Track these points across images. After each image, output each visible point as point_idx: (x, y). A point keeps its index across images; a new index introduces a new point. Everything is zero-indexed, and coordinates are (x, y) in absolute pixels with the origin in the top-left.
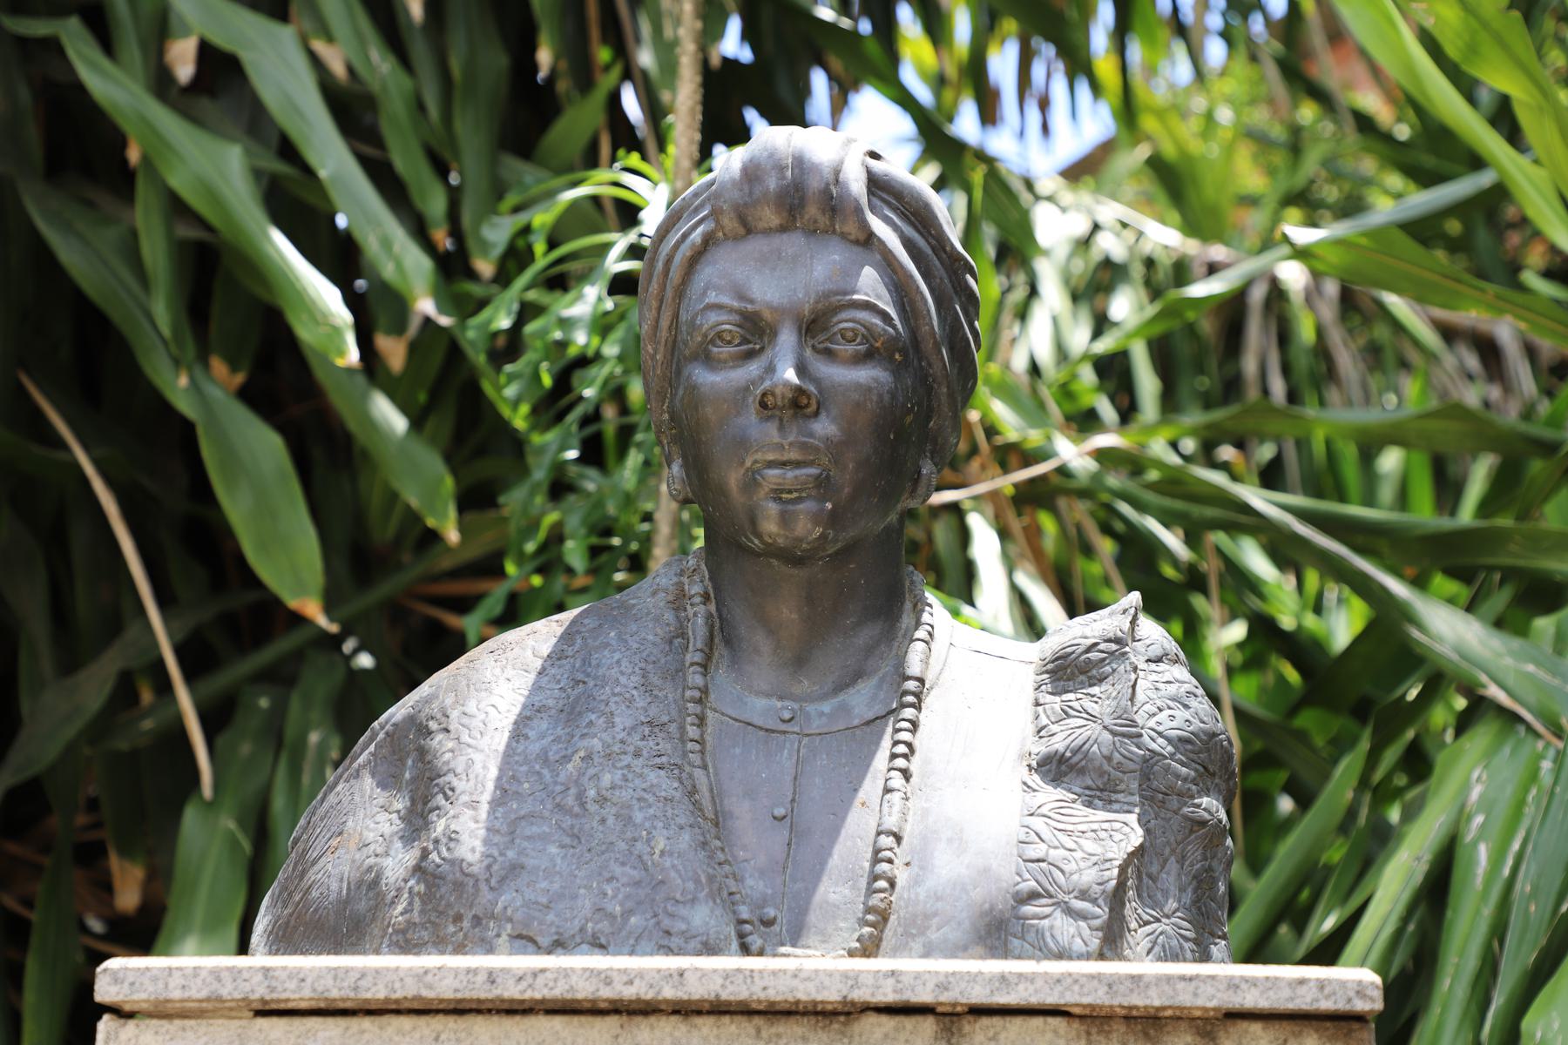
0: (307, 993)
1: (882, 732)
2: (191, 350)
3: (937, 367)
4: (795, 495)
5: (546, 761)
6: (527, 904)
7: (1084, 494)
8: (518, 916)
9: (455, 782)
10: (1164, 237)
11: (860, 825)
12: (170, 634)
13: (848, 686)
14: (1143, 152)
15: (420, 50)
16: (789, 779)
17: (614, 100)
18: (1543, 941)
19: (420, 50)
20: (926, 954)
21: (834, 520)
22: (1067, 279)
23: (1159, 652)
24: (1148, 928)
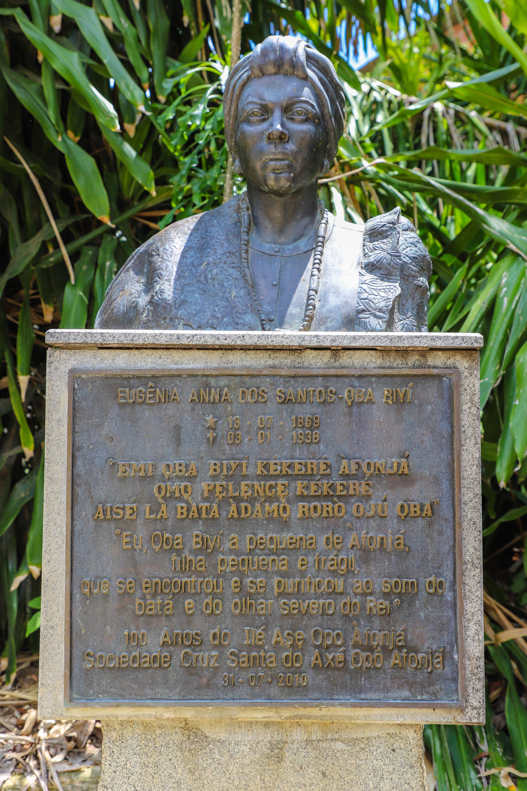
0: (116, 342)
1: (310, 256)
2: (62, 128)
3: (330, 125)
4: (280, 171)
5: (193, 265)
6: (188, 314)
7: (372, 180)
8: (185, 318)
9: (162, 272)
10: (394, 93)
11: (303, 287)
12: (58, 229)
13: (298, 240)
14: (388, 62)
15: (138, 20)
16: (278, 271)
17: (206, 41)
18: (524, 329)
19: (138, 20)
20: (326, 331)
21: (294, 180)
22: (361, 107)
23: (407, 227)
24: (401, 322)
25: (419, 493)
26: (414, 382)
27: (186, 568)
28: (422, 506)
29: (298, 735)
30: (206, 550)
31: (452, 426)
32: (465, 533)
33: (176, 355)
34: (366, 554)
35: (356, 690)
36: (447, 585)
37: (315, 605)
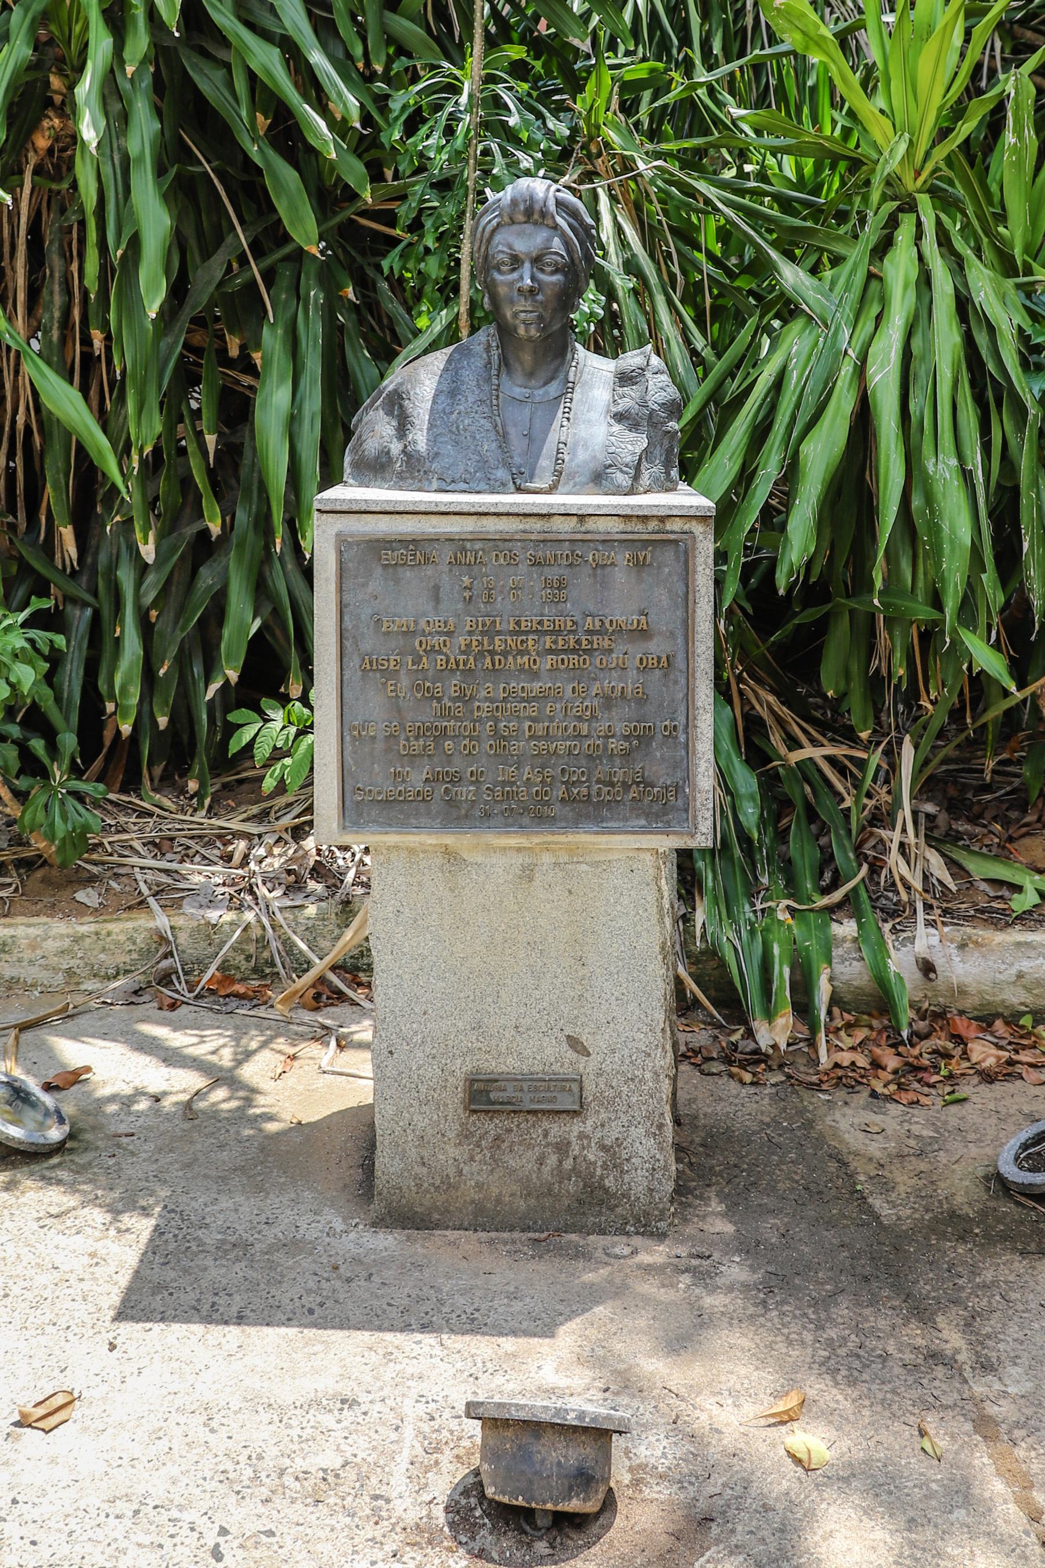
11: (553, 438)
25: (656, 647)
26: (652, 543)
27: (446, 714)
28: (659, 659)
29: (547, 859)
30: (463, 698)
31: (687, 587)
32: (698, 682)
33: (434, 519)
34: (608, 701)
35: (599, 819)
36: (681, 728)
37: (562, 746)
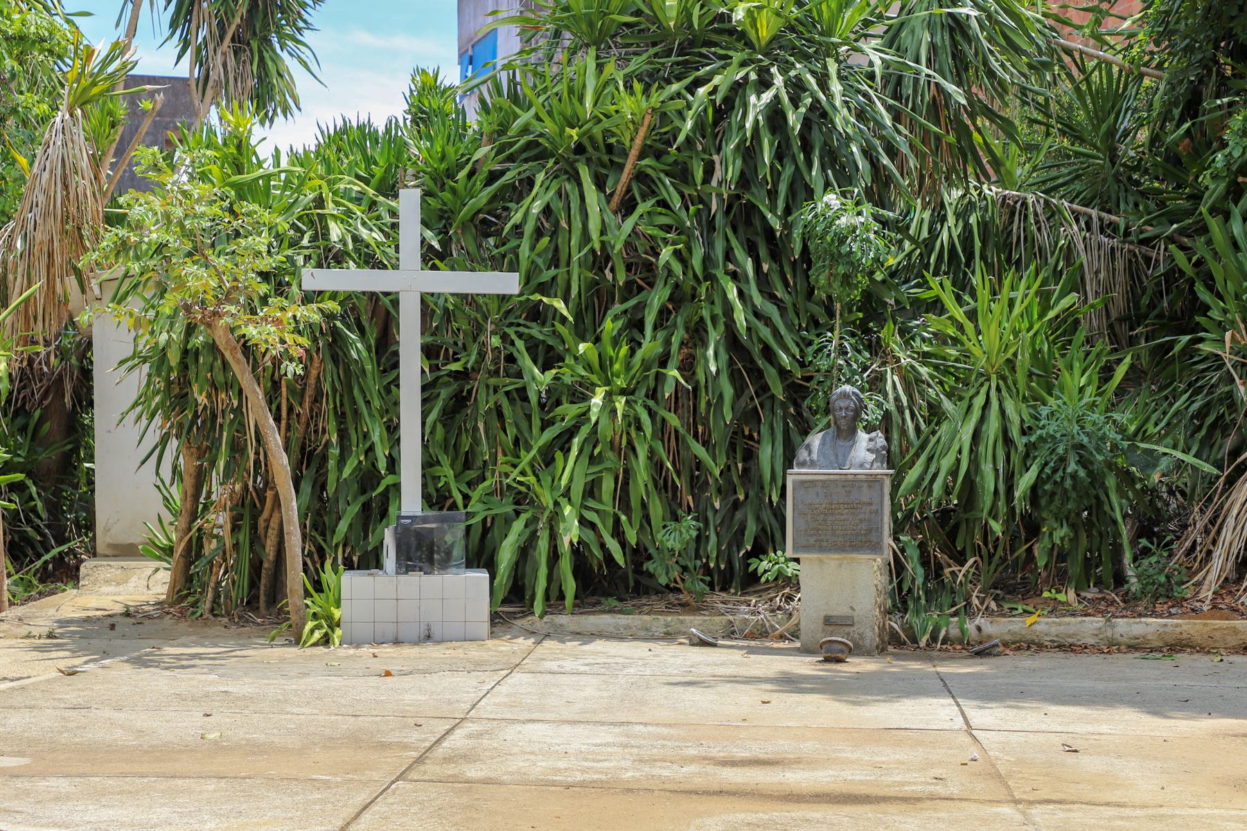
25: (874, 508)
26: (874, 481)
34: (861, 521)
